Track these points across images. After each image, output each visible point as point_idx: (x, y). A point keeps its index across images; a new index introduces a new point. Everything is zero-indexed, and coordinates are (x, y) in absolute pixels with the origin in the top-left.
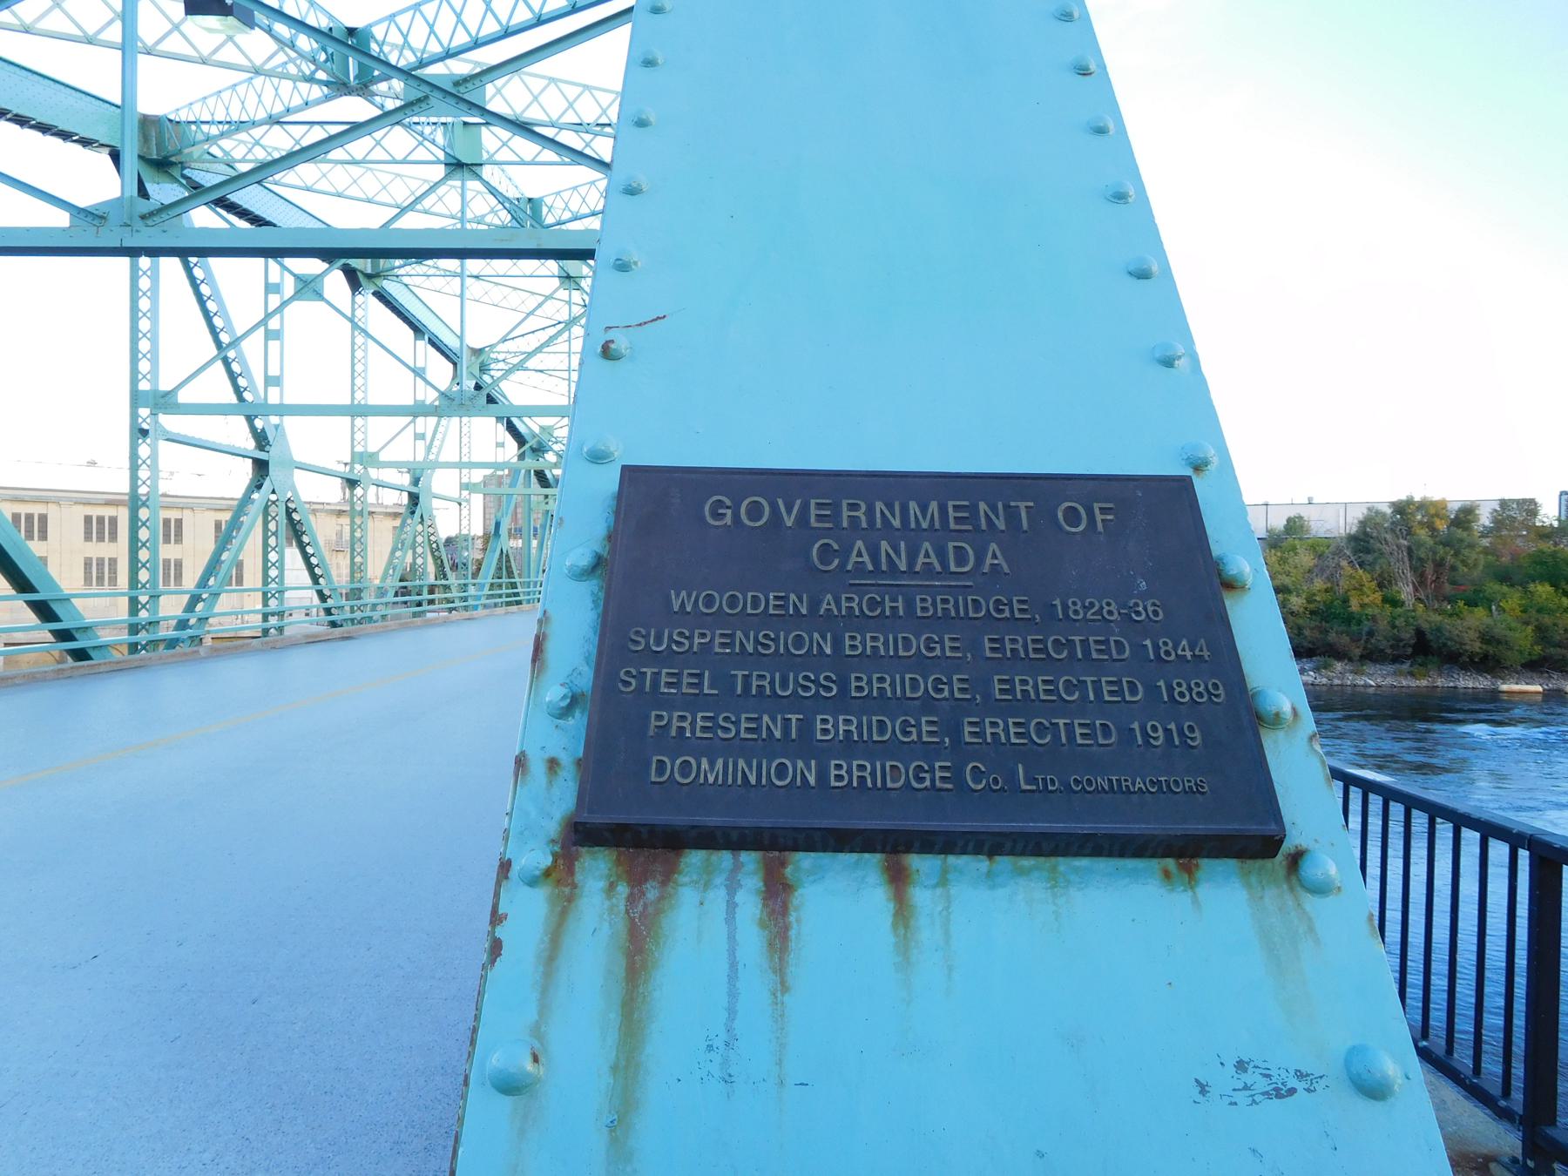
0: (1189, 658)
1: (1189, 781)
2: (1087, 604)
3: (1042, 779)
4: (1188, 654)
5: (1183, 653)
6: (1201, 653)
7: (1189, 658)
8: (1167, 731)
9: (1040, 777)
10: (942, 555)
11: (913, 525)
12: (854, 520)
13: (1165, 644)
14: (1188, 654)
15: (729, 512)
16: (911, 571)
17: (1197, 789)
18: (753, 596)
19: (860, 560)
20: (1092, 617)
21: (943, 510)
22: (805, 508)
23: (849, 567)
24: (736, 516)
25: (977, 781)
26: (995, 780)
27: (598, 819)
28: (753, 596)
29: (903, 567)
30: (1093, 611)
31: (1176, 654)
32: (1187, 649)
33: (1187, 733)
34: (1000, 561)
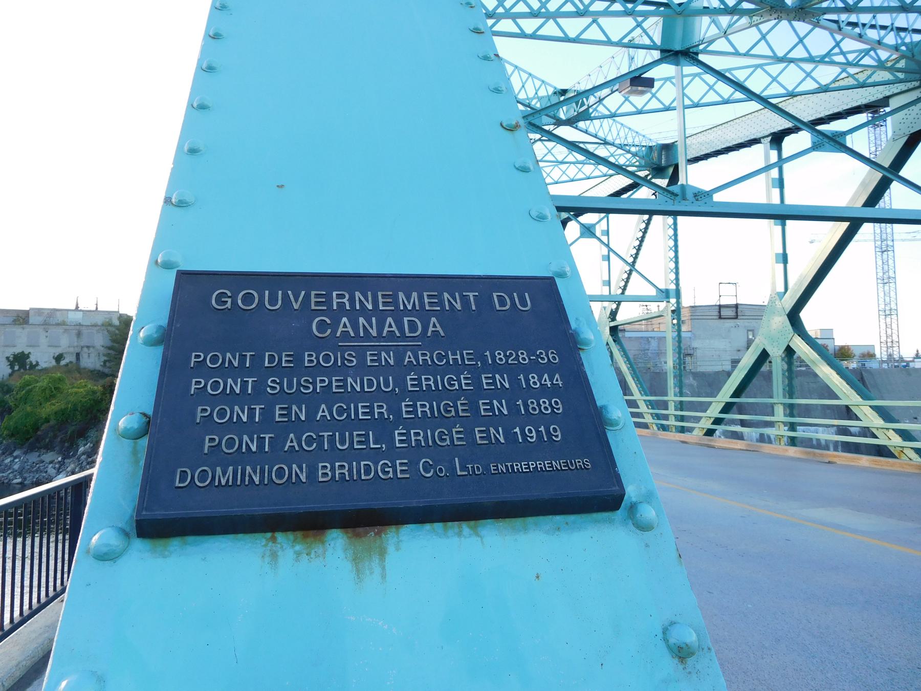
0: (549, 386)
1: (579, 462)
2: (508, 354)
3: (471, 467)
4: (549, 383)
5: (557, 383)
6: (546, 383)
7: (549, 386)
8: (538, 432)
9: (470, 466)
10: (401, 328)
11: (402, 308)
12: (341, 305)
13: (533, 377)
14: (549, 383)
15: (229, 300)
16: (380, 337)
17: (584, 466)
18: (269, 355)
19: (346, 330)
20: (513, 362)
21: (421, 298)
22: (307, 297)
23: (338, 335)
24: (234, 303)
25: (427, 471)
26: (441, 470)
27: (159, 513)
28: (269, 355)
29: (374, 333)
30: (512, 358)
31: (541, 384)
32: (548, 380)
33: (552, 433)
34: (439, 328)
